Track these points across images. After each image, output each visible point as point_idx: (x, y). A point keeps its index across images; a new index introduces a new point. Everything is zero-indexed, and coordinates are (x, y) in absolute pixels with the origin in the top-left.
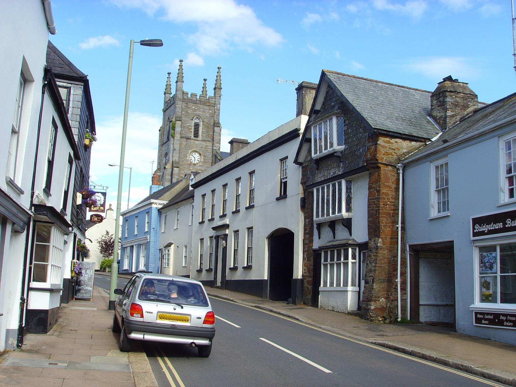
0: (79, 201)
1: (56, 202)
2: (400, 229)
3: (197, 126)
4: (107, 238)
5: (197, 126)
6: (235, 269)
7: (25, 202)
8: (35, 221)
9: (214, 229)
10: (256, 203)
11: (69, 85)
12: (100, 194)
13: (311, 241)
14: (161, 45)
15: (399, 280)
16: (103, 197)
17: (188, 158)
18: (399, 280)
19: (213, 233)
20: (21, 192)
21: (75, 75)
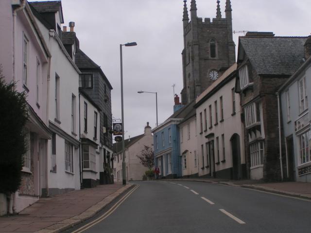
0: (105, 131)
1: (90, 136)
2: (280, 129)
3: (213, 47)
4: (149, 153)
5: (213, 47)
6: (218, 163)
7: (78, 138)
8: (82, 144)
9: (206, 137)
10: (224, 118)
11: (91, 73)
12: (119, 125)
13: (248, 140)
14: (136, 45)
15: (281, 158)
16: (121, 126)
17: (207, 76)
18: (281, 158)
19: (207, 140)
20: (76, 135)
21: (94, 67)
